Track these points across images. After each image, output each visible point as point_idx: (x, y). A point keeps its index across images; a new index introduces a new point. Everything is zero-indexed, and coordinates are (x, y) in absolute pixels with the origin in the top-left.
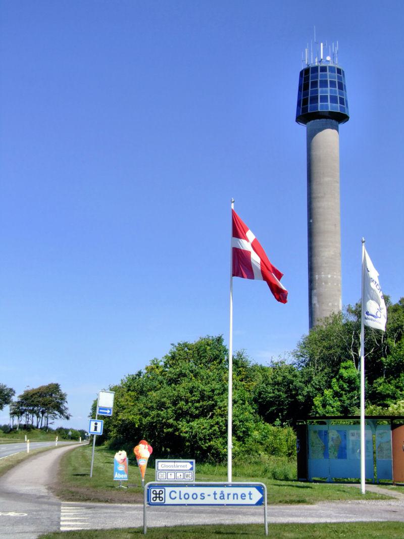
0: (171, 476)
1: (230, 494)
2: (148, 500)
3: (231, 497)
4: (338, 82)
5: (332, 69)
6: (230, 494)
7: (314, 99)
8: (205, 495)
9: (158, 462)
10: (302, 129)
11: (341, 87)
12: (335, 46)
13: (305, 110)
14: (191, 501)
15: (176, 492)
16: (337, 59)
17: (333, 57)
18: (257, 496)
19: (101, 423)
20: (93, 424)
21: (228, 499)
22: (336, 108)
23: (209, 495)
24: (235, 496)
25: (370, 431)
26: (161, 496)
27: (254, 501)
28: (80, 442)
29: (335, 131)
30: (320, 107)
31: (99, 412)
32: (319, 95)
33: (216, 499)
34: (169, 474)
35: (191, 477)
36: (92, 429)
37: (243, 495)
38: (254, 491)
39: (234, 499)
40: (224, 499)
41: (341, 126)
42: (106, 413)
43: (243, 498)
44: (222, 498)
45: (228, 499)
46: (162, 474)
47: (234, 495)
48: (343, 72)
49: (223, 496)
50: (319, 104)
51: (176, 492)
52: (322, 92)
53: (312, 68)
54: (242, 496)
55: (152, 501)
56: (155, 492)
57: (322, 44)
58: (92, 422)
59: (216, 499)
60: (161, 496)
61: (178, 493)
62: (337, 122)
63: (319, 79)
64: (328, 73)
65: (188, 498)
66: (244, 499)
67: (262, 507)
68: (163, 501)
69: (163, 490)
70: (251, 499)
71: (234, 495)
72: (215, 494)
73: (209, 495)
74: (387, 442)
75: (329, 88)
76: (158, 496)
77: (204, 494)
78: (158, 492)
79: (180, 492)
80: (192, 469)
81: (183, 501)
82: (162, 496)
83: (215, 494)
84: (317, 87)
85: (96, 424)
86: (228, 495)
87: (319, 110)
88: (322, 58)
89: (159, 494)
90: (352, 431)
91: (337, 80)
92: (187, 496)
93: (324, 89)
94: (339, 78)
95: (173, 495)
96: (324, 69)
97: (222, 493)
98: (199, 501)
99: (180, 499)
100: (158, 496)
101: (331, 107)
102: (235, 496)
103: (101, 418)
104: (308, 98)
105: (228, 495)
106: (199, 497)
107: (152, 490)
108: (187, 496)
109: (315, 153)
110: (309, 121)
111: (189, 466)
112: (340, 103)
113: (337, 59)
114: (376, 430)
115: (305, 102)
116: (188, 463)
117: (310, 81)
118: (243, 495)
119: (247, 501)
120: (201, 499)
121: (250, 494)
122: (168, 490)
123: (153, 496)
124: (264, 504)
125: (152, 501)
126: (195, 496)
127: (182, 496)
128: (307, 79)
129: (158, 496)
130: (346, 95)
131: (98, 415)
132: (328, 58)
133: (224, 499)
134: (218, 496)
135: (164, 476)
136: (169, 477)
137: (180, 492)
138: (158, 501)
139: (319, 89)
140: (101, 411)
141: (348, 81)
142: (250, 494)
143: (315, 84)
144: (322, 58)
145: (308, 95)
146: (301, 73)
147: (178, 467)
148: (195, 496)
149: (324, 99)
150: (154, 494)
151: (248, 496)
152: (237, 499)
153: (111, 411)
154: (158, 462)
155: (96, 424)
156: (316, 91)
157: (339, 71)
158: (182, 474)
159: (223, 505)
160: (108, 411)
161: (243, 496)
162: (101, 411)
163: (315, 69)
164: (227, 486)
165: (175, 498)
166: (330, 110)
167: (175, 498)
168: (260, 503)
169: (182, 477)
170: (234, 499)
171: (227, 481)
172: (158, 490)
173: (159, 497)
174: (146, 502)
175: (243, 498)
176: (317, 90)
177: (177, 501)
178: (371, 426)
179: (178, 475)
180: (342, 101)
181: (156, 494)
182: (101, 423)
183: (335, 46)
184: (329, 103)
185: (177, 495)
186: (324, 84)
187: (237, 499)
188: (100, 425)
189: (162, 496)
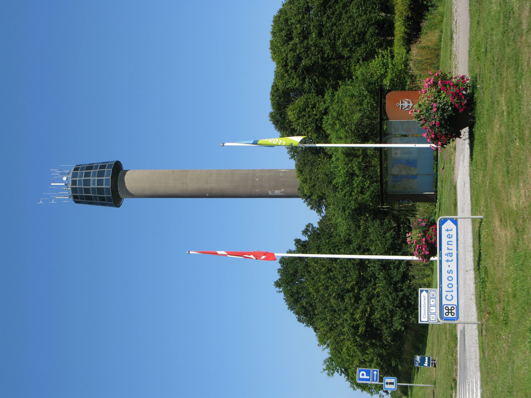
0: (433, 310)
1: (448, 248)
2: (454, 320)
3: (450, 247)
4: (85, 170)
5: (74, 175)
6: (448, 248)
7: (100, 191)
8: (449, 269)
9: (421, 321)
10: (126, 202)
11: (90, 167)
12: (54, 172)
13: (109, 199)
14: (454, 282)
15: (447, 295)
16: (65, 171)
17: (64, 174)
18: (449, 225)
19: (394, 388)
20: (388, 387)
21: (452, 249)
22: (108, 171)
23: (449, 266)
24: (449, 243)
25: (392, 139)
26: (450, 308)
27: (454, 227)
28: (383, 383)
29: (128, 173)
30: (106, 186)
31: (376, 381)
32: (96, 186)
33: (452, 260)
34: (431, 311)
35: (434, 292)
36: (393, 387)
37: (449, 236)
38: (444, 227)
39: (452, 244)
40: (452, 253)
41: (125, 168)
42: (377, 375)
43: (451, 236)
44: (451, 255)
45: (452, 249)
46: (431, 318)
47: (448, 244)
48: (77, 166)
49: (450, 253)
50: (104, 186)
51: (447, 295)
52: (94, 184)
53: (72, 193)
54: (450, 238)
55: (455, 316)
56: (447, 314)
57: (52, 184)
58: (386, 388)
59: (452, 260)
60: (450, 308)
61: (447, 293)
62: (121, 171)
63: (82, 187)
64: (77, 179)
65: (451, 277)
66: (452, 235)
67: (459, 221)
68: (455, 307)
69: (445, 306)
70: (452, 229)
71: (448, 244)
72: (448, 261)
73: (449, 266)
74: (402, 125)
75: (91, 178)
76: (450, 311)
77: (448, 271)
78: (447, 311)
79: (446, 291)
80: (427, 291)
81: (455, 288)
82: (450, 307)
83: (448, 261)
84: (90, 188)
85: (387, 383)
86: (448, 249)
87: (110, 187)
88: (64, 184)
89: (448, 310)
90: (393, 155)
91: (84, 171)
92: (450, 286)
93: (91, 182)
94: (82, 169)
95: (449, 297)
96: (74, 183)
97: (446, 255)
98: (454, 275)
99: (452, 291)
100: (450, 311)
101: (107, 178)
102: (449, 243)
103: (381, 380)
104: (98, 196)
105: (448, 249)
106: (450, 275)
107: (445, 316)
108: (450, 286)
109: (147, 192)
110: (119, 195)
111: (424, 294)
112: (105, 168)
113: (65, 171)
114: (392, 134)
115: (102, 199)
116: (422, 294)
117: (84, 194)
118: (449, 236)
119: (454, 233)
120: (452, 273)
121: (447, 230)
122: (445, 302)
123: (450, 315)
124: (456, 219)
125: (455, 316)
126: (450, 279)
127: (450, 290)
128: (82, 197)
129: (450, 311)
130: (97, 163)
131: (379, 382)
132: (65, 179)
133: (452, 253)
134: (450, 259)
135: (433, 316)
136: (434, 311)
137: (446, 291)
138: (454, 311)
139: (92, 186)
140: (375, 380)
141: (87, 161)
142: (447, 230)
143: (87, 191)
144: (64, 184)
145: (96, 196)
146: (76, 202)
147: (425, 304)
148: (450, 279)
149: (100, 182)
150: (448, 314)
151: (449, 232)
152: (452, 241)
153: (375, 370)
154: (421, 321)
155: (387, 383)
156: (93, 189)
157: (76, 169)
158: (431, 300)
159: (457, 254)
160: (375, 373)
161: (449, 236)
162: (375, 380)
163: (74, 190)
164: (441, 261)
165: (451, 295)
166: (110, 178)
167: (451, 295)
168: (455, 222)
169: (434, 300)
170: (452, 244)
171: (436, 260)
172: (445, 311)
173: (451, 310)
174: (456, 322)
175: (451, 236)
176: (92, 188)
177: (455, 294)
178: (388, 139)
179: (432, 303)
180: (103, 167)
181: (448, 313)
182: (394, 388)
183: (54, 172)
184: (104, 178)
185: (449, 294)
186: (87, 182)
187: (452, 241)
188: (388, 380)
189: (450, 307)
